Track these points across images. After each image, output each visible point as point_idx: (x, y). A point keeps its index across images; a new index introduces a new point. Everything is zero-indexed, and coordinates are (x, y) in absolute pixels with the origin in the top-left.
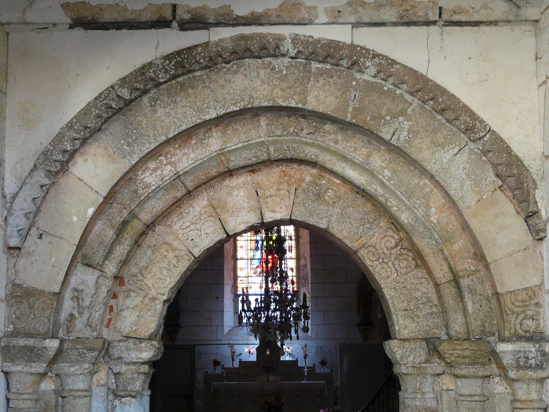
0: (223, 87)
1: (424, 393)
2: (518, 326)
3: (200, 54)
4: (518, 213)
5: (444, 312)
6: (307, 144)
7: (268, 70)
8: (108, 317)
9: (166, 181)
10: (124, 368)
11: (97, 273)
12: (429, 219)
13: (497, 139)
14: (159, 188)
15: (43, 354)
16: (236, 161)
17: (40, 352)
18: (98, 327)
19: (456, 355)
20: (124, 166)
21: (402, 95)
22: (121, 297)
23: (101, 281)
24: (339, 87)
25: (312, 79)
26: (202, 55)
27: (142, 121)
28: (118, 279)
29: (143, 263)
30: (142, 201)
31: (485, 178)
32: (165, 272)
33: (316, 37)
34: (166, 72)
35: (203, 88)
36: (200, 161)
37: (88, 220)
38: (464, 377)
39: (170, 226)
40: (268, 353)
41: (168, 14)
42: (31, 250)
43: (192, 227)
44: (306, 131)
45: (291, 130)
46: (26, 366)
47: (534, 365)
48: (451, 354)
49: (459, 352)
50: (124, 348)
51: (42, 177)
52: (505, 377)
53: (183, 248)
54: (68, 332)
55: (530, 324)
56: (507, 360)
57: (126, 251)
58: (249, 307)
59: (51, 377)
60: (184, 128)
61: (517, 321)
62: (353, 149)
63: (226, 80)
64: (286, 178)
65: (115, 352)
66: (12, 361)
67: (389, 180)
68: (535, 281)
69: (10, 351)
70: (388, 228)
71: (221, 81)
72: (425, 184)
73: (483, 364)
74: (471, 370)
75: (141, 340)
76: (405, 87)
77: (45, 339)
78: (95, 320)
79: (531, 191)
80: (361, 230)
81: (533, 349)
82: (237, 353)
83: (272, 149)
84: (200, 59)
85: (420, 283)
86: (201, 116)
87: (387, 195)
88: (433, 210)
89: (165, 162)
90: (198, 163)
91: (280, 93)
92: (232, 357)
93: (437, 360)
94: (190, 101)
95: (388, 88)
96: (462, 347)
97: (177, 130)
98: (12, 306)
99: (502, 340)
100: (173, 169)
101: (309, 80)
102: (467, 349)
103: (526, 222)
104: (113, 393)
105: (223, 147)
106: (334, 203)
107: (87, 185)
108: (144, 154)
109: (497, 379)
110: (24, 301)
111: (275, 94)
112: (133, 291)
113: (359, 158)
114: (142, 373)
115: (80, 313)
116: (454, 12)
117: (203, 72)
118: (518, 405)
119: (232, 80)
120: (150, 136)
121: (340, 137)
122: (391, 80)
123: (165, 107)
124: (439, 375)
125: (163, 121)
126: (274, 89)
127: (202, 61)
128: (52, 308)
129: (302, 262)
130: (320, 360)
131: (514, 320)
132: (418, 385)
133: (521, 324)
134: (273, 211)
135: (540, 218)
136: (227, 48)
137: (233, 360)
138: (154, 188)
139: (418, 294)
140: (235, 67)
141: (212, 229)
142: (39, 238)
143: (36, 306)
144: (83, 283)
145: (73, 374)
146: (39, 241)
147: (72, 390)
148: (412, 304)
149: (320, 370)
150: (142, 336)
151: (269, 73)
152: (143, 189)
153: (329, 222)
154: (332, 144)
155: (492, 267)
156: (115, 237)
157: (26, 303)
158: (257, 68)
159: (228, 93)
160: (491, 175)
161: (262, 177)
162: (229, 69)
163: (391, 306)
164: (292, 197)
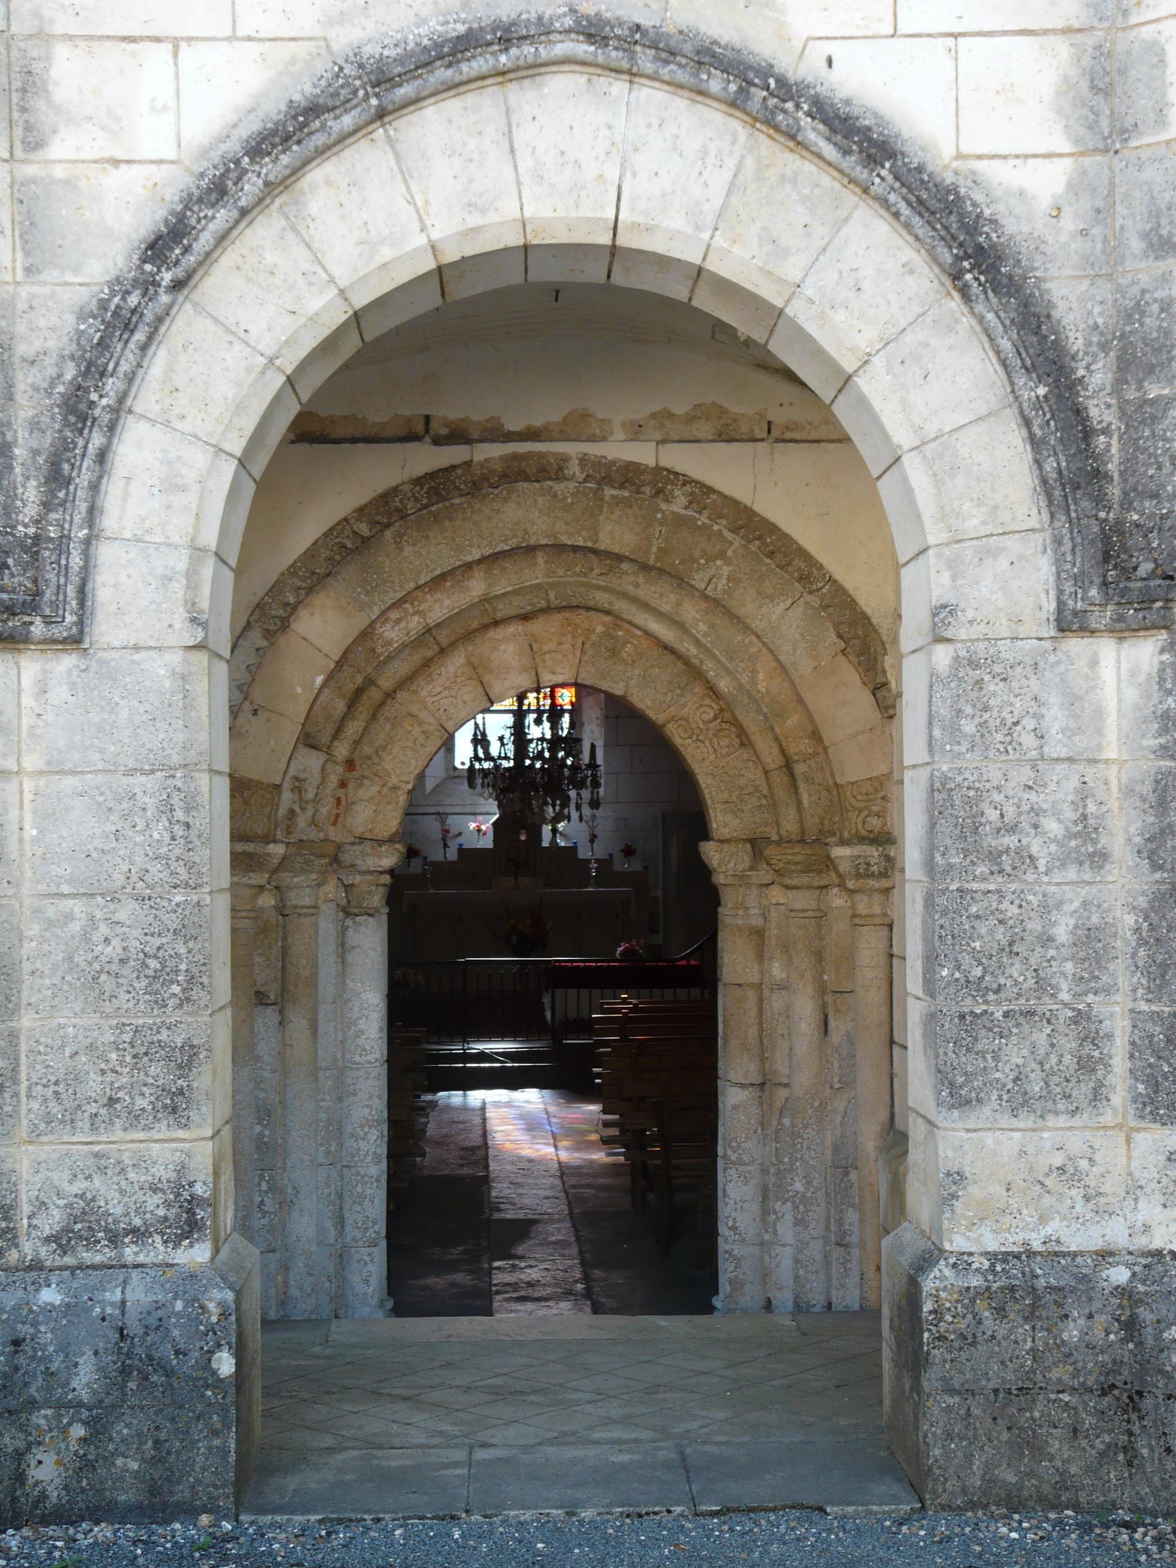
1: (747, 909)
2: (860, 826)
3: (460, 478)
4: (864, 684)
5: (774, 806)
6: (598, 587)
7: (548, 498)
8: (335, 811)
10: (358, 878)
11: (323, 757)
13: (839, 591)
14: (404, 646)
16: (504, 609)
20: (360, 622)
21: (720, 532)
22: (351, 785)
23: (329, 767)
28: (350, 764)
29: (379, 742)
32: (409, 753)
33: (610, 458)
34: (417, 500)
35: (464, 519)
38: (796, 888)
39: (415, 692)
40: (523, 838)
41: (419, 428)
42: (244, 730)
43: (445, 693)
44: (596, 571)
45: (578, 569)
52: (842, 885)
53: (432, 720)
54: (289, 833)
55: (874, 822)
56: (844, 867)
58: (487, 753)
60: (438, 572)
63: (492, 510)
65: (346, 858)
67: (706, 635)
68: (882, 769)
70: (705, 695)
72: (751, 642)
73: (820, 872)
74: (804, 879)
75: (381, 842)
76: (724, 522)
77: (267, 843)
79: (879, 658)
80: (669, 698)
81: (876, 854)
82: (454, 831)
83: (552, 594)
85: (747, 768)
86: (462, 557)
87: (701, 656)
88: (761, 676)
89: (411, 611)
92: (444, 839)
93: (765, 866)
99: (843, 842)
101: (602, 511)
102: (799, 853)
103: (874, 695)
106: (633, 661)
109: (835, 890)
111: (557, 530)
112: (367, 778)
113: (666, 608)
114: (381, 885)
115: (303, 809)
116: (787, 428)
117: (463, 499)
118: (858, 921)
121: (641, 580)
122: (706, 513)
124: (767, 885)
127: (462, 487)
130: (622, 846)
132: (740, 898)
133: (864, 823)
134: (553, 673)
135: (889, 690)
137: (446, 846)
139: (743, 782)
141: (472, 695)
144: (305, 771)
145: (297, 886)
146: (253, 719)
147: (296, 907)
148: (735, 795)
149: (622, 865)
150: (380, 837)
153: (627, 687)
154: (631, 588)
155: (830, 751)
156: (346, 709)
160: (832, 634)
161: (536, 626)
162: (497, 496)
163: (707, 796)
164: (578, 653)
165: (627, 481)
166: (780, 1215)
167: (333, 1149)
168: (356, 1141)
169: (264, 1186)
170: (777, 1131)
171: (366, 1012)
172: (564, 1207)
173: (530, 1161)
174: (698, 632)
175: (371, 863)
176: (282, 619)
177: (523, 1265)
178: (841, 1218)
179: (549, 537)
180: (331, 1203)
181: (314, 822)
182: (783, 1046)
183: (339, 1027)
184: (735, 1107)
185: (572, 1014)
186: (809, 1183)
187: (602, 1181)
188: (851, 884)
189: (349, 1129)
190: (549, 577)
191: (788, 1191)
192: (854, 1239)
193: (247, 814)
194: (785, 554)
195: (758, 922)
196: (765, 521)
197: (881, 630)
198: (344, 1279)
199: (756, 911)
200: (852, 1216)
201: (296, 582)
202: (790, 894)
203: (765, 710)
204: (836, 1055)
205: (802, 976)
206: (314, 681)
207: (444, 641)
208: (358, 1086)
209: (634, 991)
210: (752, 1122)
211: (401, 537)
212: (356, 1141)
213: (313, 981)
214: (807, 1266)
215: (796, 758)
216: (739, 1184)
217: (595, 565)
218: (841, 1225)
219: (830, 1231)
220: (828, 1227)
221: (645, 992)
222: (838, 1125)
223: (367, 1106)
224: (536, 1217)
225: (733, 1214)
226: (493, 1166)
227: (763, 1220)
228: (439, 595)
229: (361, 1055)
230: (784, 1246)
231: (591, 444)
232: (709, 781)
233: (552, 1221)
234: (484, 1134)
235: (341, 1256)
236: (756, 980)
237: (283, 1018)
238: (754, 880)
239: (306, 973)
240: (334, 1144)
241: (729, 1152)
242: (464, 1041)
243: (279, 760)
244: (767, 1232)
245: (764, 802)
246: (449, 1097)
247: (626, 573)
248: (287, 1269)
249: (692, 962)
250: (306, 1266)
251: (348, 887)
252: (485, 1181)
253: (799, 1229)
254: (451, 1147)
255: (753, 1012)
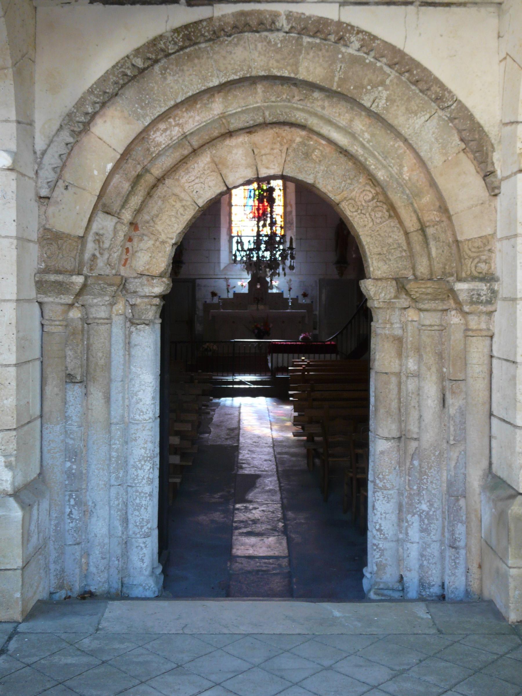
0: (225, 58)
1: (392, 324)
2: (473, 269)
3: (205, 28)
4: (478, 172)
6: (297, 109)
7: (265, 43)
8: (124, 257)
9: (174, 140)
10: (139, 301)
11: (115, 220)
12: (402, 176)
13: (462, 107)
14: (168, 147)
15: (71, 288)
16: (235, 124)
17: (68, 286)
18: (116, 266)
19: (420, 292)
20: (139, 127)
22: (135, 240)
24: (327, 59)
25: (303, 52)
26: (207, 28)
27: (153, 87)
28: (133, 225)
29: (154, 212)
30: (153, 158)
31: (451, 141)
32: (173, 219)
34: (175, 43)
35: (208, 58)
36: (205, 124)
37: (107, 174)
38: (426, 310)
39: (178, 180)
40: (258, 287)
42: (59, 200)
43: (197, 181)
44: (297, 98)
45: (284, 97)
46: (57, 298)
47: (484, 301)
48: (416, 292)
49: (424, 290)
50: (138, 284)
51: (67, 136)
52: (460, 309)
53: (189, 199)
54: (91, 270)
55: (483, 266)
56: (462, 297)
57: (140, 201)
58: (242, 248)
59: (77, 307)
60: (190, 94)
61: (473, 265)
62: (338, 114)
63: (227, 52)
64: (279, 139)
65: (131, 287)
66: (45, 293)
67: (368, 142)
68: (489, 231)
69: (43, 285)
70: (366, 183)
71: (223, 53)
72: (399, 146)
73: (443, 300)
75: (153, 277)
76: (384, 60)
77: (72, 275)
78: (114, 260)
79: (490, 154)
80: (343, 185)
81: (485, 288)
82: (231, 286)
83: (267, 113)
84: (205, 32)
85: (393, 231)
87: (366, 155)
88: (406, 169)
90: (203, 124)
91: (275, 64)
92: (228, 289)
93: (404, 296)
94: (195, 70)
95: (370, 61)
96: (425, 286)
97: (184, 95)
98: (43, 247)
99: (460, 280)
100: (180, 130)
102: (430, 287)
103: (484, 180)
104: (130, 321)
105: (225, 111)
106: (320, 161)
107: (106, 143)
108: (156, 116)
110: (53, 243)
112: (146, 235)
113: (343, 122)
114: (154, 305)
117: (207, 44)
118: (470, 333)
119: (233, 52)
120: (161, 101)
121: (326, 104)
122: (372, 54)
123: (174, 75)
124: (405, 309)
125: (172, 88)
126: (269, 60)
127: (206, 34)
128: (77, 250)
129: (289, 209)
130: (302, 293)
131: (470, 263)
132: (388, 317)
133: (476, 267)
134: (267, 168)
135: (496, 176)
136: (228, 23)
137: (228, 292)
138: (164, 146)
139: (390, 241)
140: (236, 40)
141: (214, 182)
142: (65, 189)
143: (64, 247)
144: (103, 228)
145: (96, 305)
146: (65, 192)
147: (95, 318)
148: (385, 249)
149: (302, 301)
150: (154, 274)
151: (265, 46)
152: (154, 147)
153: (315, 177)
154: (319, 109)
156: (130, 189)
157: (55, 245)
158: (255, 41)
159: (230, 64)
163: (367, 250)
164: (284, 155)
165: (318, 31)
166: (410, 523)
167: (121, 475)
168: (136, 470)
169: (72, 502)
170: (410, 469)
171: (143, 387)
172: (274, 467)
173: (259, 437)
174: (364, 139)
175: (147, 290)
176: (84, 123)
177: (251, 507)
178: (453, 530)
179: (265, 70)
180: (119, 510)
181: (108, 263)
182: (414, 415)
183: (126, 396)
184: (382, 453)
185: (280, 365)
186: (432, 505)
187: (293, 450)
188: (466, 308)
189: (131, 462)
190: (265, 102)
191: (416, 508)
192: (462, 544)
193: (61, 256)
194: (426, 82)
195: (398, 332)
196: (412, 60)
197: (490, 136)
198: (128, 558)
199: (398, 325)
200: (461, 529)
201: (94, 99)
202: (422, 315)
203: (408, 192)
204: (452, 422)
205: (429, 369)
206: (106, 167)
207: (195, 144)
208: (138, 435)
209: (307, 355)
210: (393, 462)
211: (165, 70)
212: (136, 470)
213: (108, 366)
214: (429, 559)
215: (428, 224)
216: (384, 502)
217: (296, 94)
218: (453, 534)
219: (444, 536)
220: (443, 534)
221: (312, 356)
222: (452, 469)
223: (144, 448)
224: (260, 473)
225: (380, 521)
226: (242, 440)
227: (399, 525)
228: (192, 113)
229: (140, 415)
230: (412, 543)
231: (295, 4)
232: (368, 239)
233: (267, 476)
234: (239, 421)
235: (126, 543)
236: (397, 370)
237: (87, 391)
238: (398, 305)
239: (102, 362)
240: (122, 472)
241: (378, 481)
242: (233, 375)
243: (82, 220)
244: (401, 533)
245: (404, 254)
246: (226, 400)
247: (317, 99)
248: (89, 555)
249: (333, 343)
250: (101, 553)
251: (133, 306)
252: (236, 449)
253: (424, 534)
254: (223, 428)
255: (395, 391)
